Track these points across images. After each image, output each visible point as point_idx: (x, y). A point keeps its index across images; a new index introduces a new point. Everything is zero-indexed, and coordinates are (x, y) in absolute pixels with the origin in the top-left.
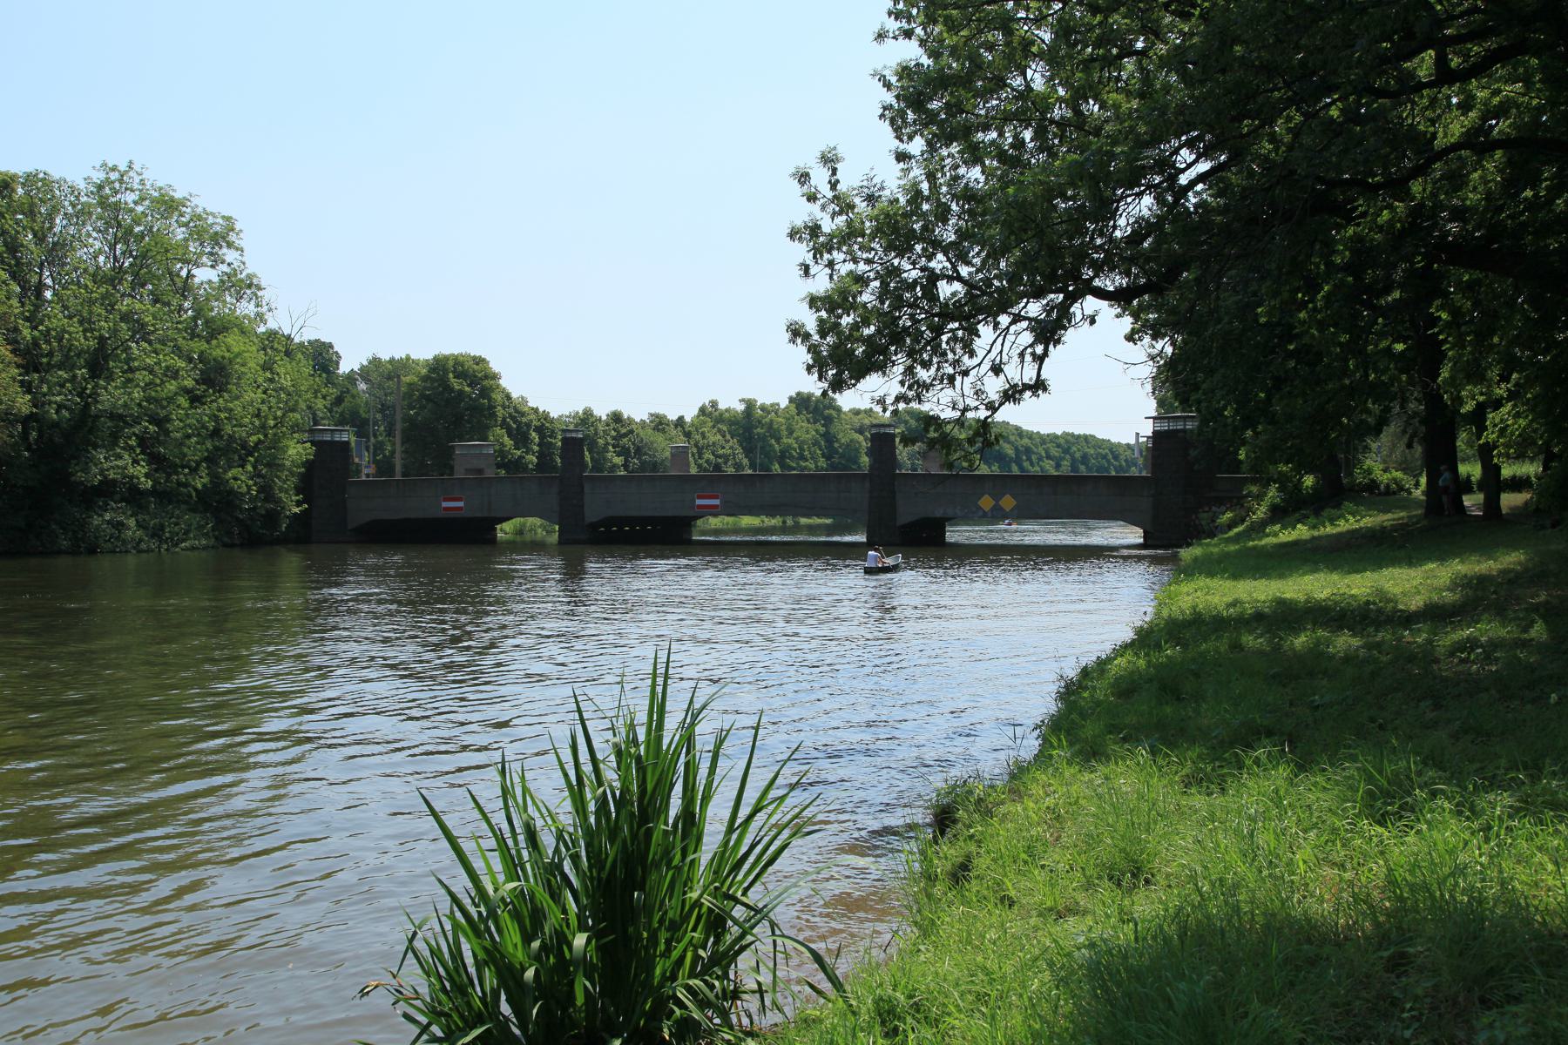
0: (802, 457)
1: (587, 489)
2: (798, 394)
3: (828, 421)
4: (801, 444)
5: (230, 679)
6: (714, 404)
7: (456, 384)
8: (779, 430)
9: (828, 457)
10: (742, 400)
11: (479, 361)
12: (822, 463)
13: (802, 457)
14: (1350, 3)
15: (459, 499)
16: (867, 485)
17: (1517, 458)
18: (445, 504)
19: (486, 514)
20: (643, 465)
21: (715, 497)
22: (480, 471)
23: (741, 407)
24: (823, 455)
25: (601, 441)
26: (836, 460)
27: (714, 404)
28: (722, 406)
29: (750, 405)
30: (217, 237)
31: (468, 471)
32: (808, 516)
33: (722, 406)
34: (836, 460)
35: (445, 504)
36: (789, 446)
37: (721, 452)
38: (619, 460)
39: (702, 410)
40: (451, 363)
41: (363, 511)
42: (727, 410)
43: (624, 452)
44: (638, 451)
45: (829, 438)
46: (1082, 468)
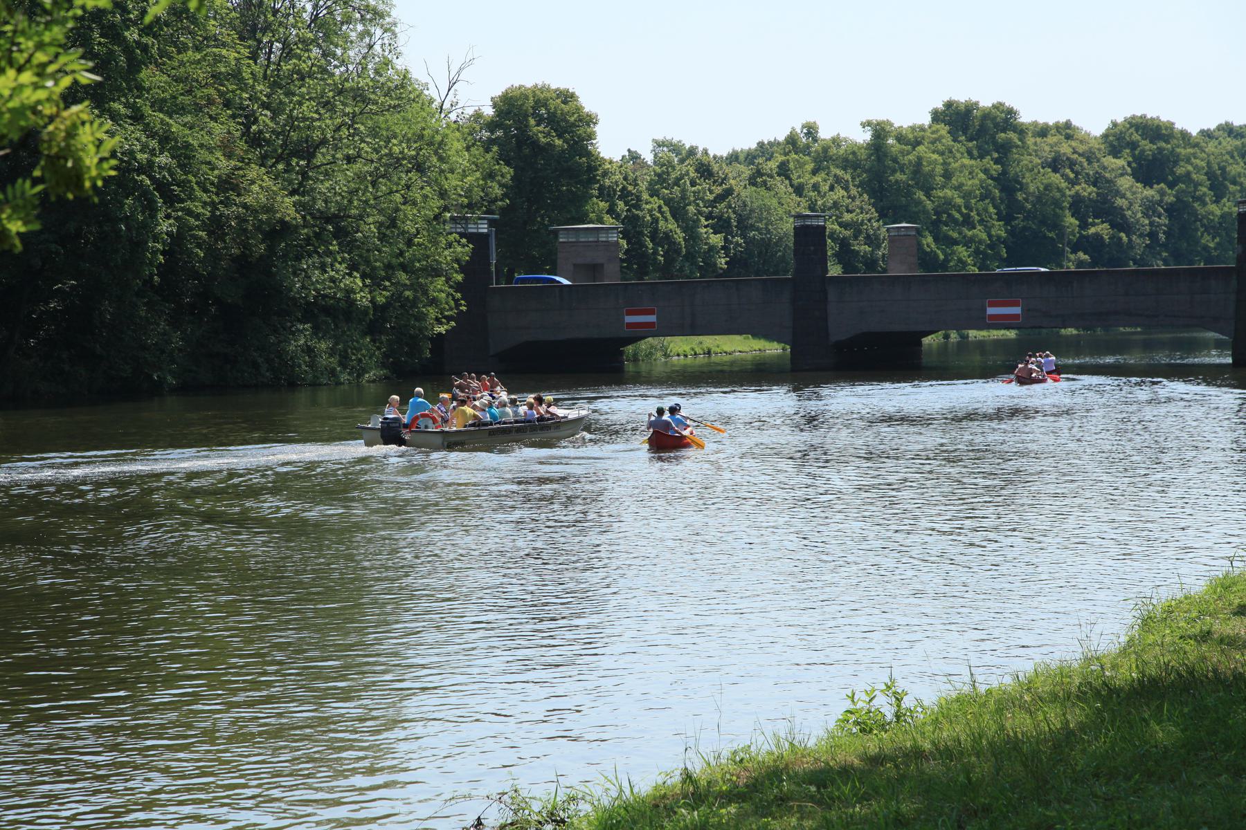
0: (968, 222)
1: (832, 295)
2: (949, 105)
3: (1004, 150)
4: (967, 196)
6: (811, 130)
7: (539, 131)
8: (931, 175)
9: (1006, 218)
11: (567, 97)
12: (999, 230)
15: (651, 312)
18: (629, 319)
23: (863, 137)
25: (691, 209)
26: (1019, 222)
28: (825, 134)
29: (880, 131)
30: (1115, 124)
32: (1124, 327)
33: (825, 134)
34: (1019, 222)
35: (629, 319)
36: (949, 202)
37: (847, 217)
38: (716, 240)
40: (531, 102)
42: (836, 141)
43: (721, 226)
44: (741, 220)
45: (1008, 184)
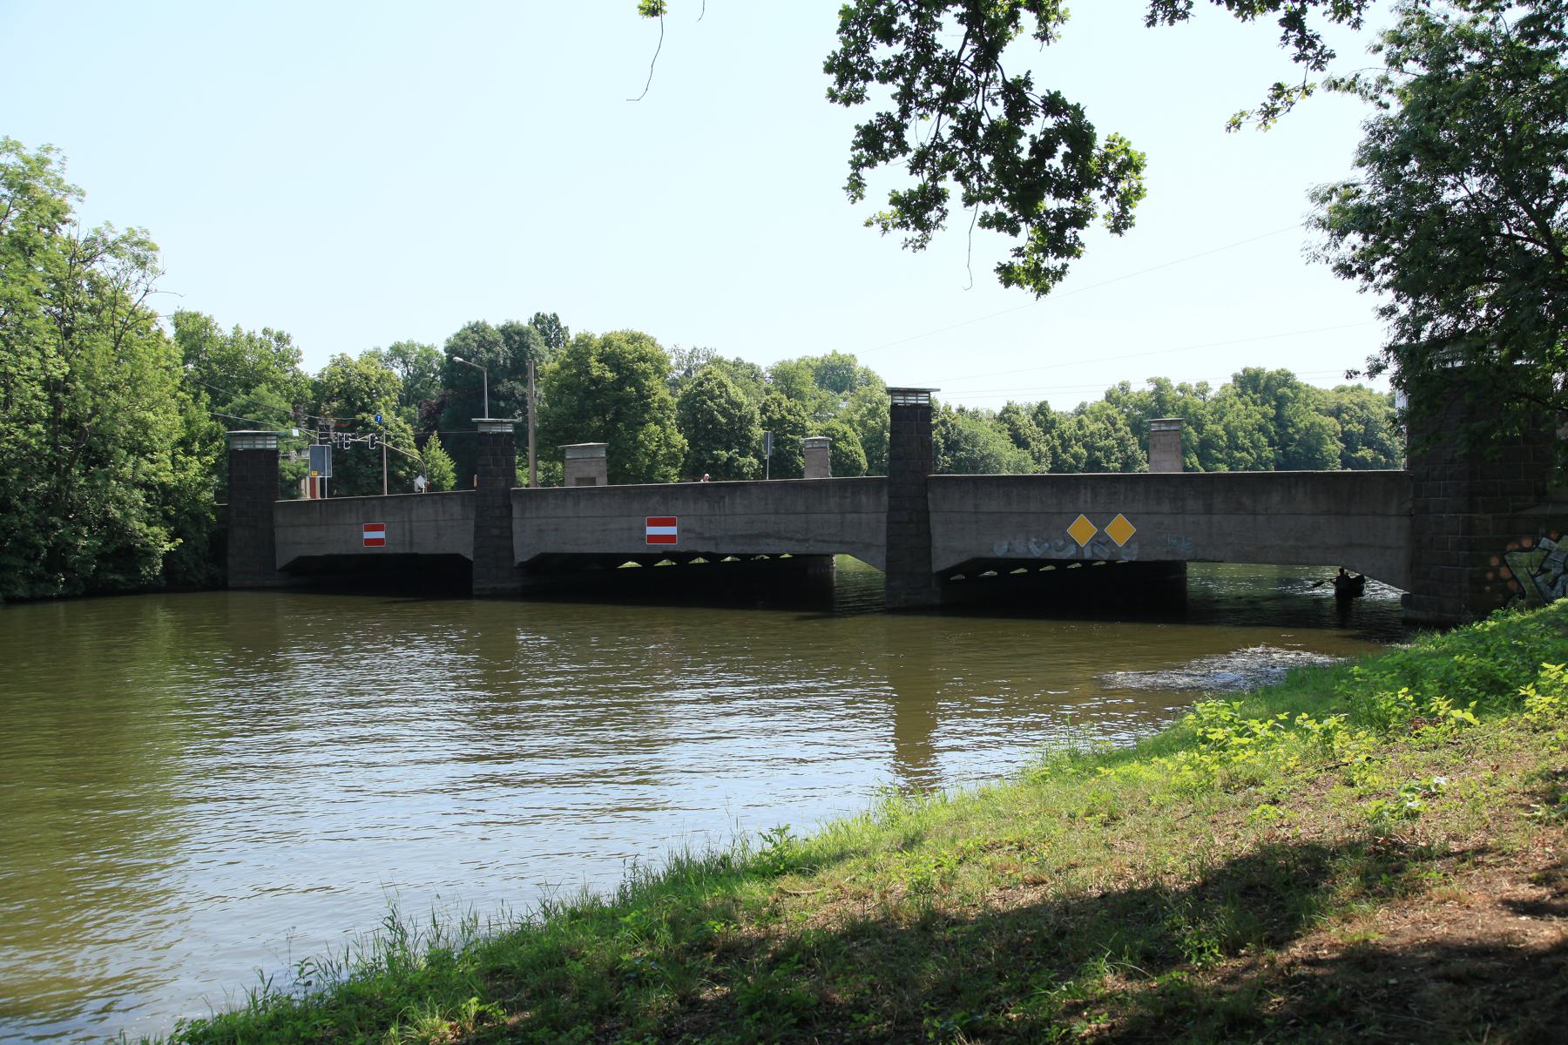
5: (1312, 666)
6: (1124, 387)
10: (1150, 381)
12: (1268, 453)
13: (1234, 445)
14: (1564, 48)
16: (885, 498)
17: (1427, 612)
19: (407, 551)
20: (958, 465)
21: (670, 523)
22: (593, 481)
23: (1151, 388)
24: (1271, 443)
27: (1124, 387)
29: (1160, 386)
31: (579, 481)
39: (1110, 397)
41: (296, 541)
46: (1366, 453)
